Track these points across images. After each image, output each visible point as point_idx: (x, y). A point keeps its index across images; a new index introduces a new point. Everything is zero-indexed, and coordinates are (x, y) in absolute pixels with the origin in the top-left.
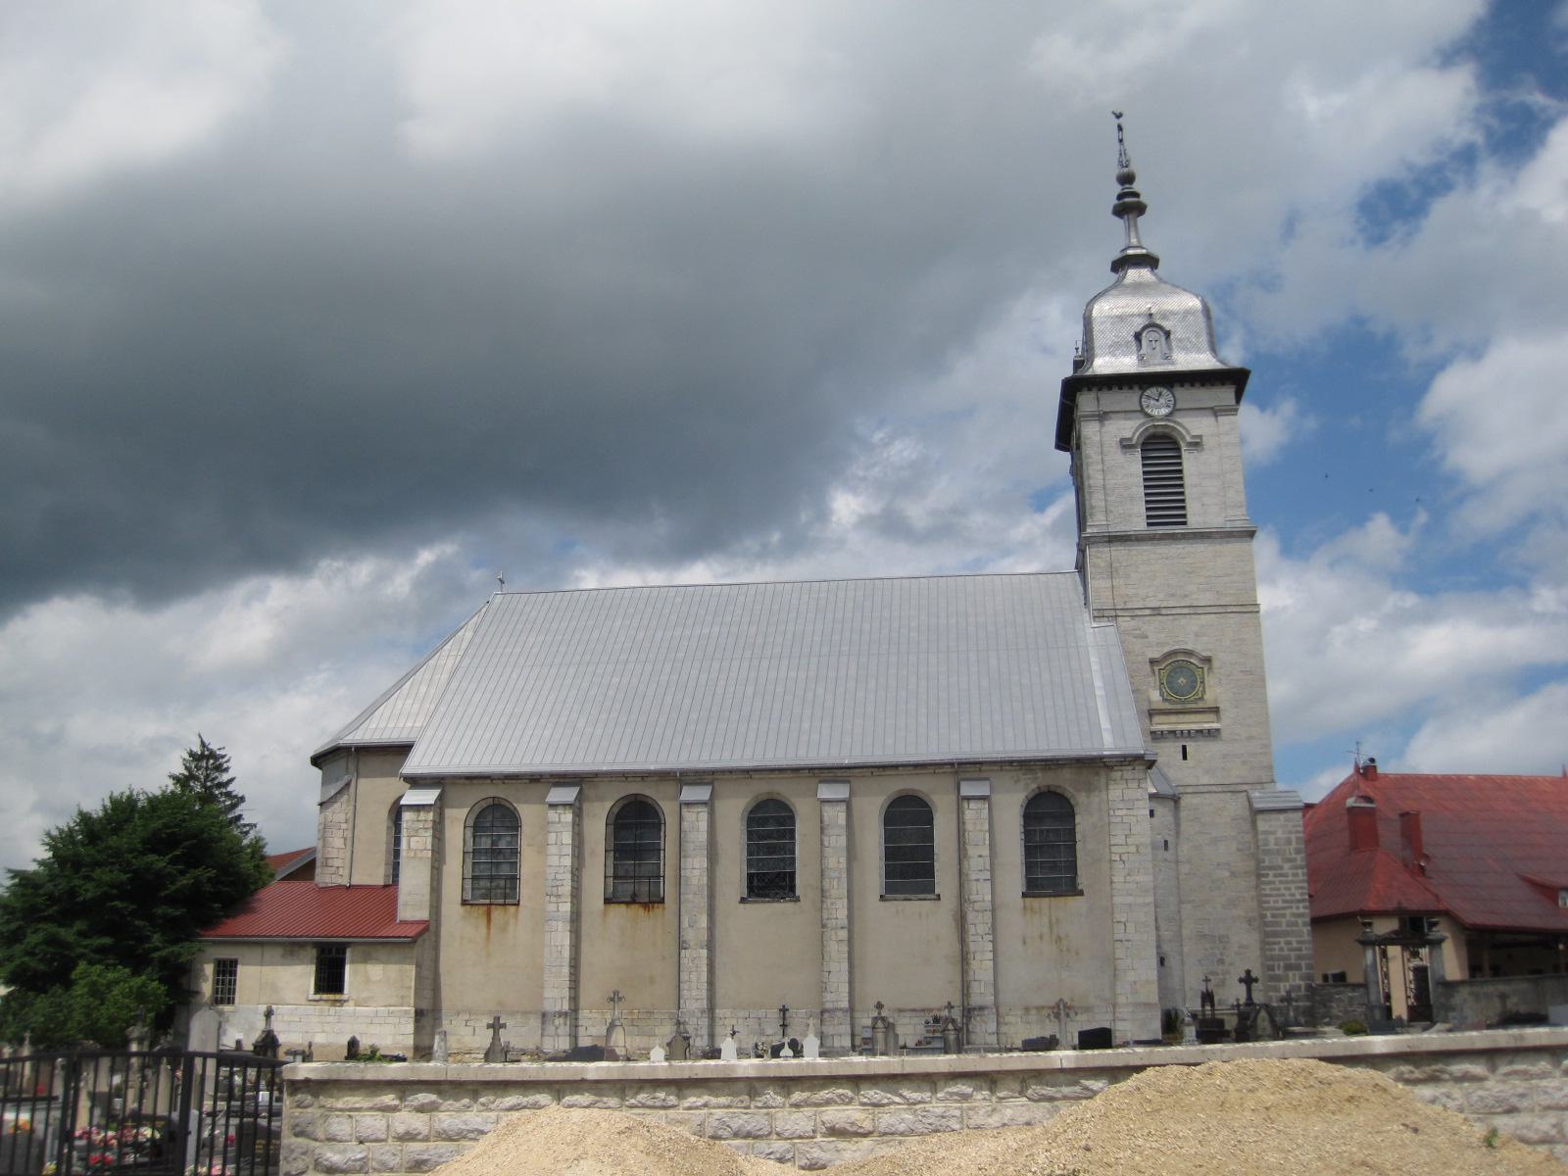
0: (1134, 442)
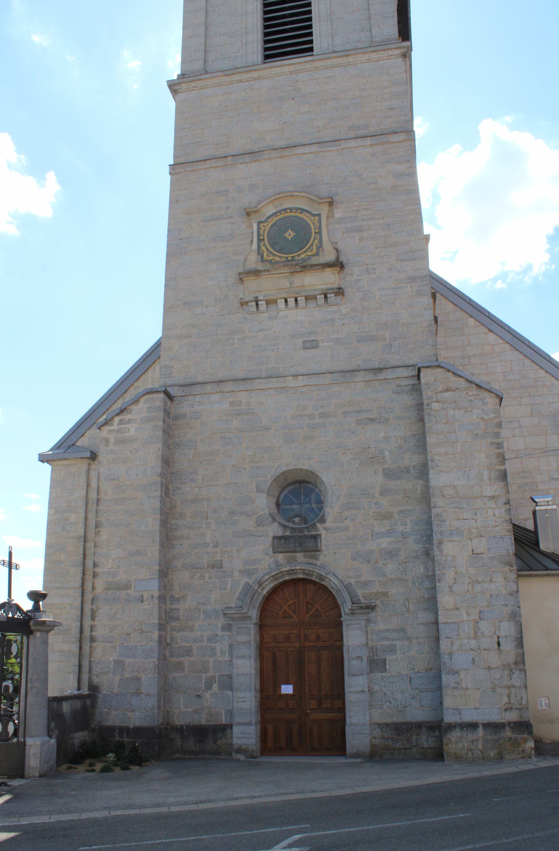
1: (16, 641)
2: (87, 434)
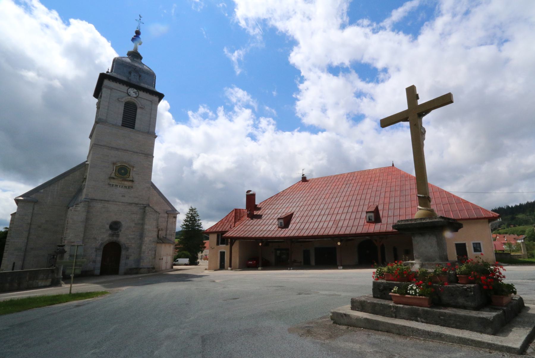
0: (123, 100)
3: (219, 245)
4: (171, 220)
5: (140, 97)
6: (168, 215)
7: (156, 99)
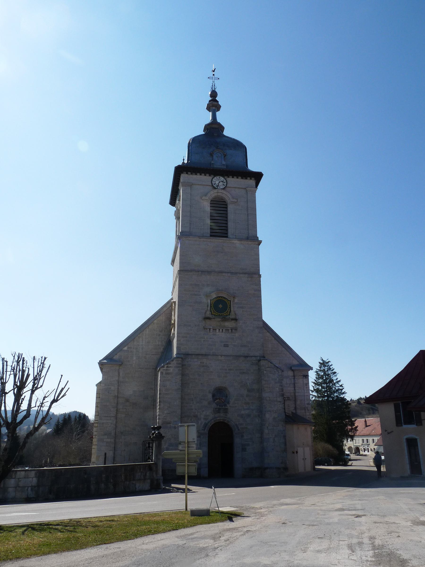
1: (151, 443)
2: (118, 354)
3: (402, 426)
4: (300, 381)
5: (229, 187)
6: (294, 371)
7: (252, 182)
